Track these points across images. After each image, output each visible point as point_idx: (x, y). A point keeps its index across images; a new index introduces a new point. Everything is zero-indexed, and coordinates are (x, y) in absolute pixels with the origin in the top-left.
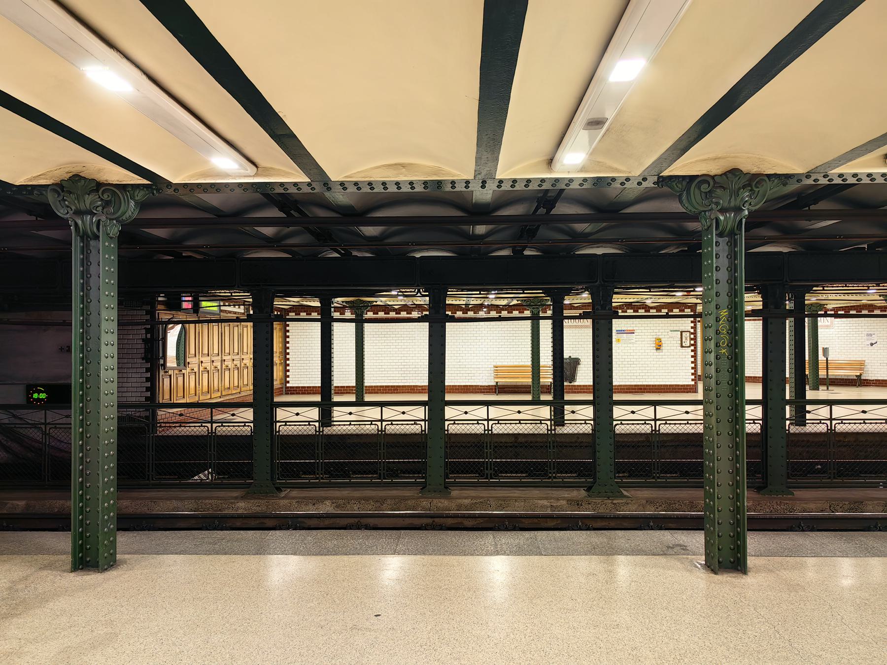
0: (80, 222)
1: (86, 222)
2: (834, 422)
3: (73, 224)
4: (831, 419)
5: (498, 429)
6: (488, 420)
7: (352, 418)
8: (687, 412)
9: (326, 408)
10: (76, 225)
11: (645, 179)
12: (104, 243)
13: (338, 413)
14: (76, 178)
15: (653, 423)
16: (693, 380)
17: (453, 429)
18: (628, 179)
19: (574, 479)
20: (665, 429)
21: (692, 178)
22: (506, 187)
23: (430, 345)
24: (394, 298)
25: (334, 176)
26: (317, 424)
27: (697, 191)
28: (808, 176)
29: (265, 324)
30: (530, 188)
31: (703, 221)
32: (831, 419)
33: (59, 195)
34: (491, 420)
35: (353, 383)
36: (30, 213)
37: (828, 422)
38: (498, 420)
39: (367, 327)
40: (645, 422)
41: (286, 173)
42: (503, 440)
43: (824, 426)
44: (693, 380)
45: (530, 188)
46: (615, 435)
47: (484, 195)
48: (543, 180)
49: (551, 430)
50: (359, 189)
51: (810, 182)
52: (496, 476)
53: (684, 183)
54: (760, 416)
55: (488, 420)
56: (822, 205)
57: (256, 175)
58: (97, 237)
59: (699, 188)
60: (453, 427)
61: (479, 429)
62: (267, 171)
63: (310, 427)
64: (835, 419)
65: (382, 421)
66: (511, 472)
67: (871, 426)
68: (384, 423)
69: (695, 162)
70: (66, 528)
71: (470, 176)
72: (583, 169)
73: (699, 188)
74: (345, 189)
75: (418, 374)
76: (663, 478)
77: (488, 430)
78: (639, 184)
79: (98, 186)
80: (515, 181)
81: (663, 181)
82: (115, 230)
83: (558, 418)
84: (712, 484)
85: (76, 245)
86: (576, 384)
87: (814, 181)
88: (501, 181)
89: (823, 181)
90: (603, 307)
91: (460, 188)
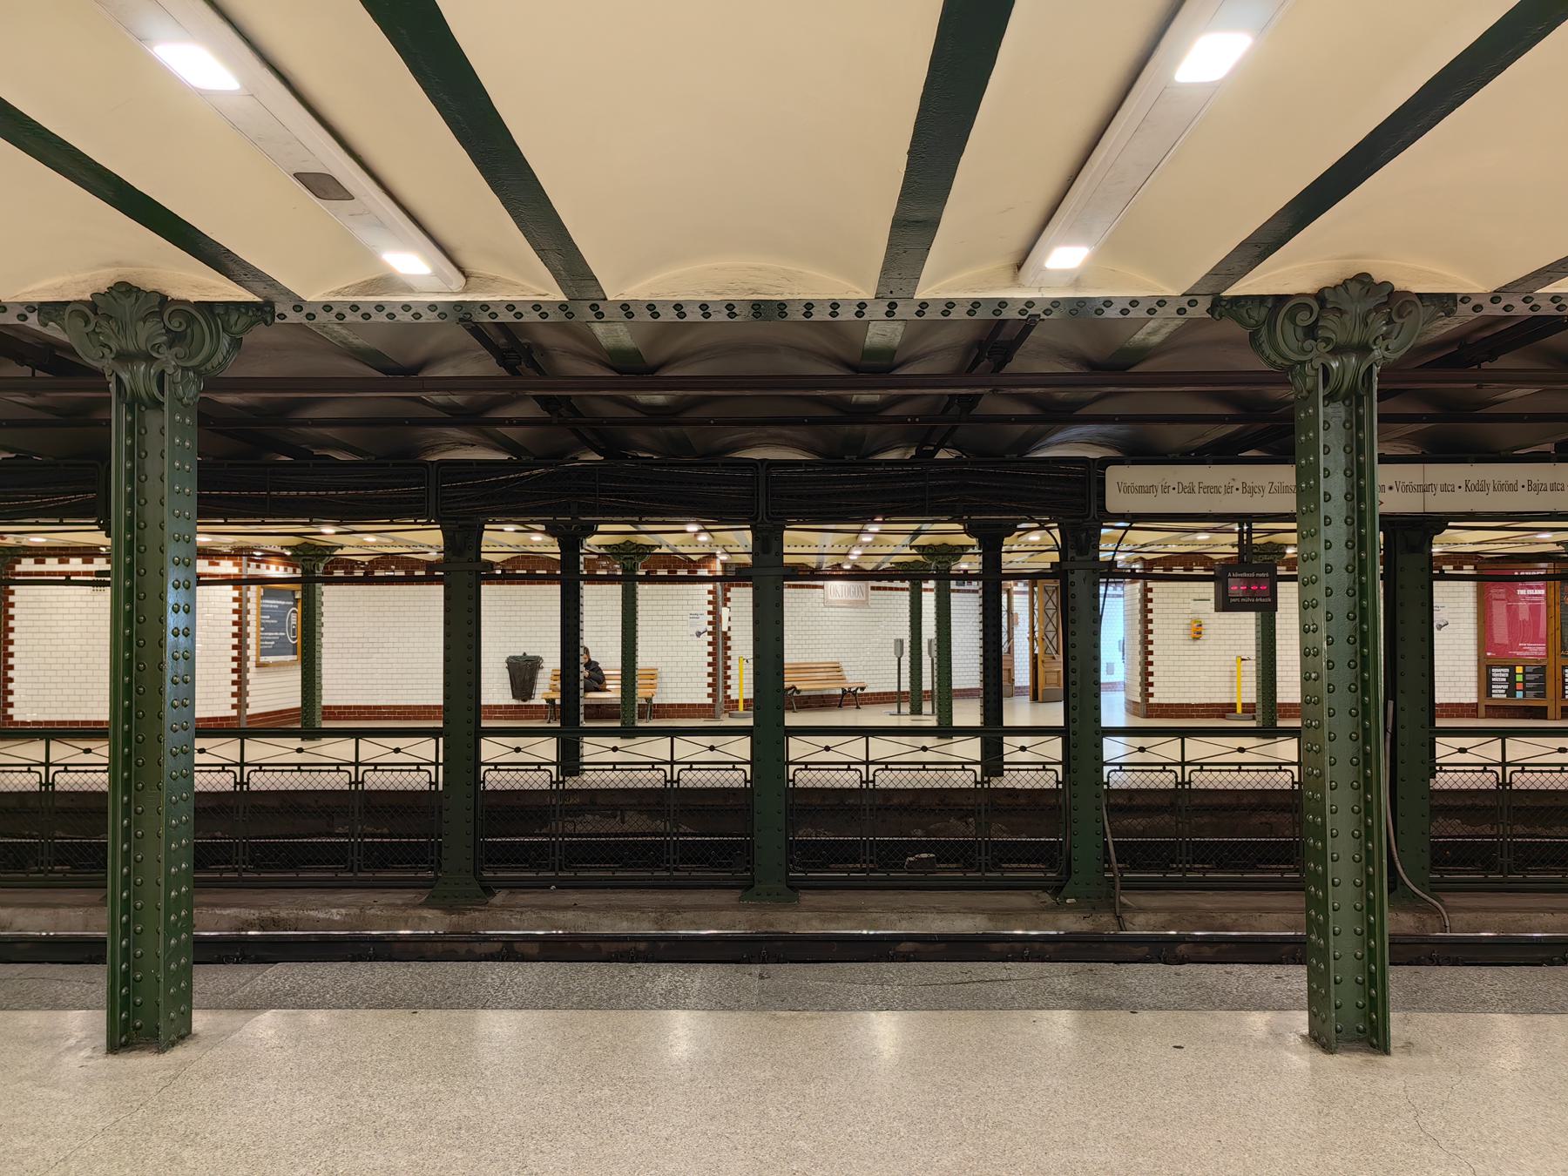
0: (125, 377)
1: (138, 377)
2: (1509, 769)
3: (113, 379)
4: (242, 764)
5: (885, 780)
6: (1183, 764)
7: (298, 758)
8: (1241, 750)
9: (769, 738)
10: (119, 380)
11: (1192, 303)
12: (172, 415)
13: (593, 749)
14: (124, 289)
15: (42, 770)
16: (709, 695)
17: (804, 779)
18: (1134, 303)
19: (1063, 875)
20: (1521, 781)
21: (1281, 299)
22: (932, 314)
23: (447, 635)
24: (686, 537)
25: (615, 290)
26: (553, 769)
27: (1289, 328)
28: (1495, 298)
29: (463, 580)
30: (951, 317)
31: (1298, 382)
32: (47, 764)
33: (87, 322)
34: (873, 763)
35: (432, 693)
36: (21, 361)
37: (1499, 769)
38: (261, 765)
39: (643, 590)
40: (653, 765)
41: (520, 280)
42: (1225, 801)
43: (545, 776)
44: (709, 695)
45: (951, 317)
46: (1110, 792)
47: (882, 333)
48: (1003, 303)
49: (558, 782)
50: (655, 315)
51: (1497, 310)
52: (996, 866)
53: (1264, 312)
54: (1058, 754)
55: (672, 763)
56: (1505, 362)
57: (465, 291)
58: (159, 405)
59: (1293, 321)
60: (67, 777)
61: (850, 779)
62: (489, 282)
63: (29, 776)
64: (248, 765)
65: (672, 763)
66: (1019, 861)
67: (76, 777)
68: (677, 768)
69: (1290, 272)
70: (99, 960)
71: (867, 294)
72: (1077, 282)
73: (1293, 321)
74: (630, 315)
75: (425, 686)
76: (1198, 871)
77: (867, 782)
78: (1181, 311)
79: (162, 304)
80: (950, 304)
81: (1223, 307)
82: (191, 392)
83: (569, 760)
84: (1321, 881)
85: (118, 417)
86: (532, 702)
87: (1505, 308)
88: (924, 304)
89: (1521, 310)
90: (1082, 551)
91: (846, 315)
